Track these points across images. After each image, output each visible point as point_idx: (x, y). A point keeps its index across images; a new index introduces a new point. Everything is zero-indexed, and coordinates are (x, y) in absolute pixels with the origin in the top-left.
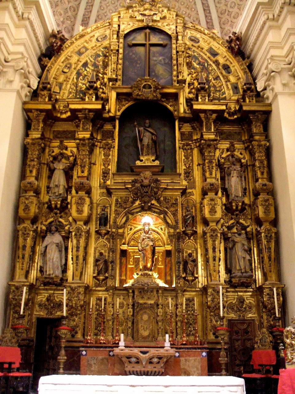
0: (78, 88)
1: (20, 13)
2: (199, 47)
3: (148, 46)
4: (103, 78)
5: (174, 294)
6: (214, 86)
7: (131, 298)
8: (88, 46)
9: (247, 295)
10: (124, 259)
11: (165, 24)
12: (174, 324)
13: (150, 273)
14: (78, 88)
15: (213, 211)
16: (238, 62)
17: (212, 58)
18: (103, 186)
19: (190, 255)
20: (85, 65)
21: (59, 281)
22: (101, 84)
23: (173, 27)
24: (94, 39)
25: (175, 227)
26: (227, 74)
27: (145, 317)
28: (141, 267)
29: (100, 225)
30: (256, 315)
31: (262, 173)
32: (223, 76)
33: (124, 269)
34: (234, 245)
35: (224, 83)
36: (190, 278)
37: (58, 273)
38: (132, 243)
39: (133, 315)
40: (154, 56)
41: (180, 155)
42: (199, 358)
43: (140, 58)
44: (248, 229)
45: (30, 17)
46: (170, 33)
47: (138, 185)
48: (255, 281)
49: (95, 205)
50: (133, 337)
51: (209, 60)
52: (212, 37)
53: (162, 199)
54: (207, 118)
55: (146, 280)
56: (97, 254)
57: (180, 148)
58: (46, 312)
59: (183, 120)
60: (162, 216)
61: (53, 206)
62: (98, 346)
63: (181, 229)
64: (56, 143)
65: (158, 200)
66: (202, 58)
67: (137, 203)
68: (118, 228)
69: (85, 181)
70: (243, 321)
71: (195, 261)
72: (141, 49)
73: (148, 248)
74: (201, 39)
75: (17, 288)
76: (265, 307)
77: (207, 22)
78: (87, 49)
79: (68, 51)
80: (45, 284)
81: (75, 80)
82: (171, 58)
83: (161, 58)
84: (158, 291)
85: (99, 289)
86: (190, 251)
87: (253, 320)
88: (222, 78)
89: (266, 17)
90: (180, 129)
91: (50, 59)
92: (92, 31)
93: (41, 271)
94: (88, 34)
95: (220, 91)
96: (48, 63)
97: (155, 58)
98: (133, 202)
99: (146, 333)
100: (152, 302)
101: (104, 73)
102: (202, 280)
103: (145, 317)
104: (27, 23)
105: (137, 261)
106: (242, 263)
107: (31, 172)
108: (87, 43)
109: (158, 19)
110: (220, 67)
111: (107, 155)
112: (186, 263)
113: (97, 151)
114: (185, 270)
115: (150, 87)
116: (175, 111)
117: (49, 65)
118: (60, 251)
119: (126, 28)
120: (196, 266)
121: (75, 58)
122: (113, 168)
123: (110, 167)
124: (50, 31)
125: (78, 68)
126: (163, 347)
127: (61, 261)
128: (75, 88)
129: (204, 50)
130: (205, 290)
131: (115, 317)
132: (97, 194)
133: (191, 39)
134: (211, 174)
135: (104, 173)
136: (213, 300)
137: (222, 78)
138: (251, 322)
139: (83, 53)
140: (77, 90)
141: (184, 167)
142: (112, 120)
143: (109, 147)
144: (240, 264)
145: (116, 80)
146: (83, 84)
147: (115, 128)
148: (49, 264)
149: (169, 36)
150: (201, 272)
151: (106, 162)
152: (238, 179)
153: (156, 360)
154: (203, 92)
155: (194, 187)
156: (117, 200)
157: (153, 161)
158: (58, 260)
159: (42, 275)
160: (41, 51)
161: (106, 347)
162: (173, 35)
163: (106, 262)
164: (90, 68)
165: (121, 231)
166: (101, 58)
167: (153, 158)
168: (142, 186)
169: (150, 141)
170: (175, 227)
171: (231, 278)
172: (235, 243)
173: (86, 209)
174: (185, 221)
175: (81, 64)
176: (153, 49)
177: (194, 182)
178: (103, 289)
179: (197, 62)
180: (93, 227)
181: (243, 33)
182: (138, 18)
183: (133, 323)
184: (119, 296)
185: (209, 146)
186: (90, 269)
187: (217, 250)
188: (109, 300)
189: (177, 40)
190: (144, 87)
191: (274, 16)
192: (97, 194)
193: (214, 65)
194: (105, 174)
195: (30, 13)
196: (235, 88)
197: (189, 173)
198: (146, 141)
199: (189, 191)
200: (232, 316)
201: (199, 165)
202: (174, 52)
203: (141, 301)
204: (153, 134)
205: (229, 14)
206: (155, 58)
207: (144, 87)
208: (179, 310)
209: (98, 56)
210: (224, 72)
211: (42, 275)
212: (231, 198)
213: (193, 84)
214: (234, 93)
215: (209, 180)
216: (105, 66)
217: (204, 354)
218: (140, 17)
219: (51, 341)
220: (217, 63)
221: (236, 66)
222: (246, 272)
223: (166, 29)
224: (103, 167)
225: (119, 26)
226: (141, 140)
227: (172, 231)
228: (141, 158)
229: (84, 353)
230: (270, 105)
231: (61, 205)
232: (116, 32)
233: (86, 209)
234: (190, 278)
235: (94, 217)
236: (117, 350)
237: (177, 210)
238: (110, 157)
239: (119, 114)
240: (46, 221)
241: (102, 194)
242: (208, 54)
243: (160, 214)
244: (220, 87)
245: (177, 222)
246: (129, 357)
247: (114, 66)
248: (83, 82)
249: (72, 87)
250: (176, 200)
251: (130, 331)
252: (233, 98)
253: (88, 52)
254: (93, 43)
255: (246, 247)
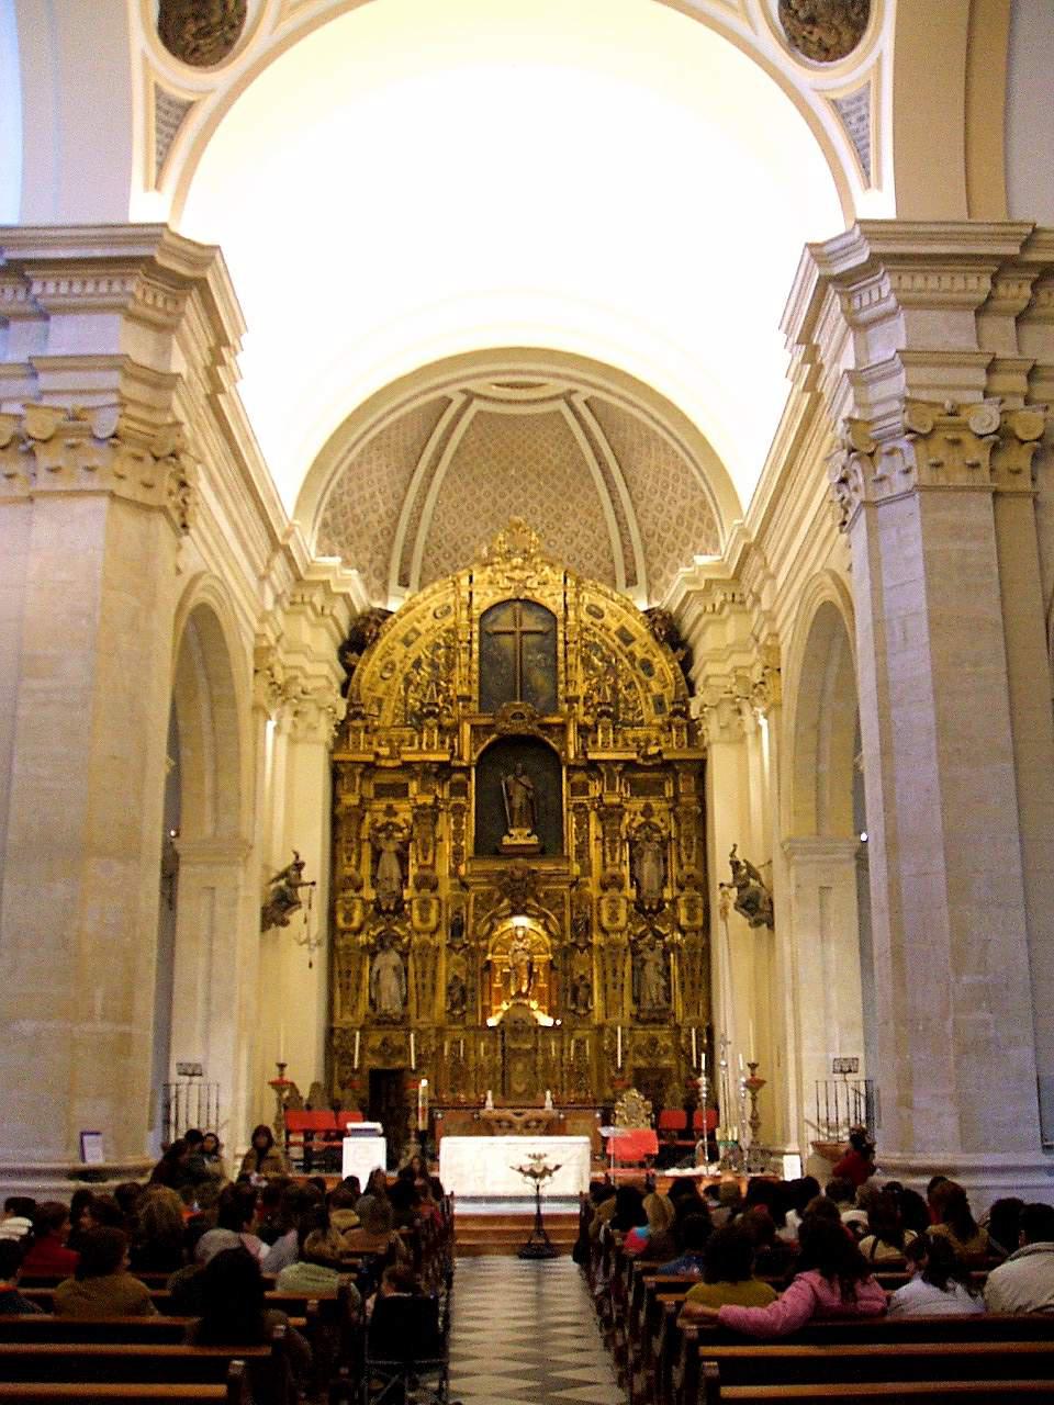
0: (409, 708)
1: (319, 609)
2: (603, 626)
3: (518, 635)
4: (447, 690)
5: (558, 1035)
6: (626, 701)
7: (499, 1042)
8: (421, 628)
9: (664, 1037)
10: (486, 975)
11: (547, 592)
12: (558, 1076)
13: (526, 1002)
14: (409, 708)
15: (614, 917)
16: (666, 653)
17: (624, 647)
18: (454, 873)
19: (582, 978)
20: (417, 664)
21: (399, 1018)
22: (444, 701)
23: (560, 599)
24: (430, 614)
25: (561, 938)
26: (646, 678)
27: (520, 1067)
28: (513, 993)
29: (452, 934)
30: (674, 1062)
31: (689, 857)
32: (641, 683)
33: (487, 991)
34: (644, 965)
35: (641, 694)
36: (582, 1011)
37: (398, 1007)
38: (498, 949)
39: (503, 1064)
40: (528, 653)
41: (571, 822)
42: (590, 1122)
43: (506, 658)
44: (667, 939)
45: (335, 612)
46: (553, 608)
47: (506, 879)
48: (674, 1015)
49: (444, 905)
50: (503, 1094)
51: (618, 652)
52: (625, 607)
53: (542, 895)
54: (610, 771)
55: (520, 1014)
56: (450, 978)
57: (568, 810)
58: (381, 1061)
59: (572, 769)
60: (542, 921)
61: (384, 908)
62: (458, 1106)
63: (569, 939)
64: (381, 805)
65: (537, 900)
66: (607, 646)
67: (506, 902)
68: (478, 939)
69: (427, 872)
70: (654, 1070)
71: (589, 987)
72: (508, 640)
73: (523, 963)
74: (606, 611)
75: (345, 1032)
76: (683, 1052)
77: (625, 557)
78: (419, 634)
79: (389, 639)
80: (378, 1023)
81: (403, 693)
82: (556, 658)
83: (539, 656)
84: (536, 1032)
85: (454, 1027)
86: (582, 972)
87: (670, 1069)
88: (638, 686)
89: (701, 608)
90: (568, 779)
91: (360, 654)
92: (425, 599)
93: (372, 1002)
94: (419, 603)
95: (633, 709)
96: (357, 661)
97: (530, 657)
98: (500, 901)
99: (520, 1089)
100: (529, 1046)
101: (449, 681)
102: (597, 1016)
103: (520, 1067)
104: (330, 621)
105: (506, 978)
106: (654, 991)
107: (349, 859)
108: (419, 622)
109: (535, 585)
110: (637, 665)
111: (458, 824)
112: (576, 990)
113: (442, 817)
114: (575, 999)
115: (522, 717)
116: (562, 750)
117: (359, 666)
118: (399, 977)
119: (482, 601)
120: (590, 993)
121: (400, 650)
122: (468, 845)
123: (463, 843)
124: (359, 610)
125: (406, 670)
126: (542, 1107)
127: (401, 989)
128: (402, 707)
129: (612, 633)
130: (600, 1029)
131: (479, 1069)
132: (446, 889)
133: (589, 612)
134: (613, 859)
135: (455, 853)
136: (610, 1043)
137: (638, 686)
138: (666, 1071)
139: (412, 642)
140: (406, 712)
141: (575, 842)
142: (466, 770)
143: (459, 811)
144: (653, 992)
145: (469, 699)
146: (416, 700)
147: (469, 779)
148: (385, 995)
149: (552, 617)
150: (597, 1001)
151: (458, 835)
152: (653, 865)
153: (534, 1124)
154: (605, 719)
155: (590, 874)
156: (476, 899)
157: (529, 835)
158: (397, 989)
159: (375, 1010)
160: (343, 636)
161: (467, 1108)
162: (560, 615)
163: (463, 990)
164: (426, 670)
165: (482, 944)
166: (442, 650)
167: (528, 831)
168: (512, 880)
169: (524, 801)
170: (561, 938)
171: (640, 1011)
172: (644, 962)
173: (433, 915)
174: (574, 928)
175: (410, 662)
176: (529, 639)
177: (590, 866)
178: (460, 1027)
179: (599, 655)
180: (442, 939)
181: (674, 609)
182: (501, 585)
183: (503, 1076)
184: (483, 1039)
185: (611, 815)
186: (441, 1001)
187: (619, 974)
188: (471, 1045)
189: (566, 619)
190: (514, 717)
191: (714, 606)
192: (446, 889)
193: (626, 661)
194: (457, 854)
195: (333, 607)
196: (659, 703)
197: (583, 851)
198: (518, 801)
199: (583, 879)
200: (641, 1063)
201: (597, 839)
202: (561, 646)
203: (513, 1046)
204: (528, 789)
205: (661, 541)
206: (530, 657)
207: (514, 717)
208: (566, 1056)
209: (438, 646)
210: (642, 674)
211: (375, 1010)
212: (644, 891)
213: (591, 697)
214: (656, 713)
215: (609, 870)
216: (450, 666)
217: (598, 1115)
218: (507, 583)
219: (388, 1101)
220: (631, 656)
221: (663, 662)
222: (659, 1003)
223: (548, 602)
224: (453, 843)
225: (471, 594)
226: (510, 798)
227: (556, 942)
228: (512, 832)
229: (440, 1116)
230: (705, 750)
231: (396, 907)
232: (465, 606)
233: (433, 915)
234: (582, 1011)
235: (443, 925)
236: (483, 1113)
237: (563, 913)
238: (464, 827)
239: (475, 758)
240: (374, 930)
241: (453, 887)
242: (617, 640)
243: (538, 917)
244: (635, 701)
245: (563, 931)
246: (499, 1121)
247: (465, 671)
248: (416, 696)
249: (399, 705)
250: (563, 897)
251: (499, 1085)
252: (655, 721)
253: (421, 639)
254: (429, 622)
255: (660, 968)
